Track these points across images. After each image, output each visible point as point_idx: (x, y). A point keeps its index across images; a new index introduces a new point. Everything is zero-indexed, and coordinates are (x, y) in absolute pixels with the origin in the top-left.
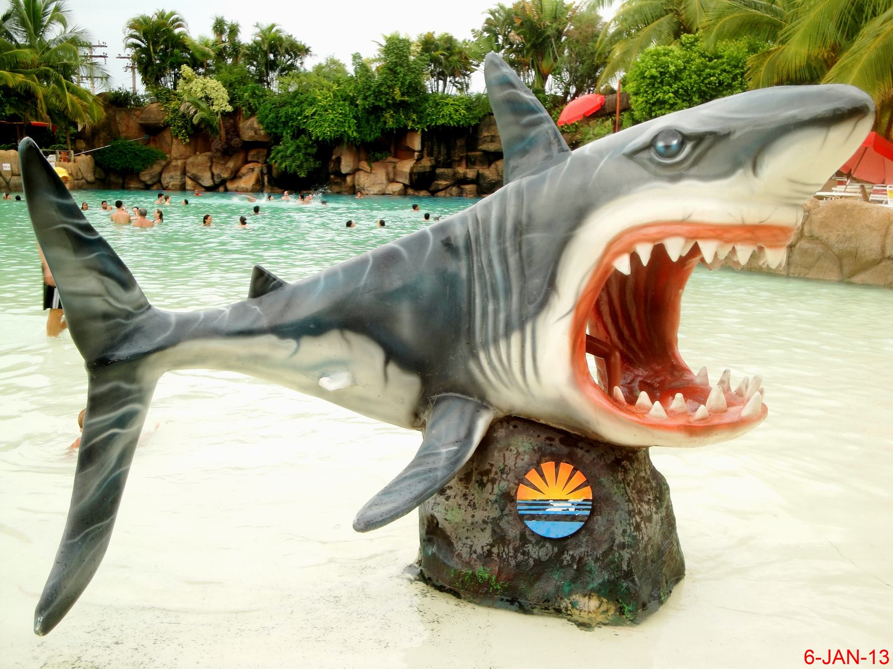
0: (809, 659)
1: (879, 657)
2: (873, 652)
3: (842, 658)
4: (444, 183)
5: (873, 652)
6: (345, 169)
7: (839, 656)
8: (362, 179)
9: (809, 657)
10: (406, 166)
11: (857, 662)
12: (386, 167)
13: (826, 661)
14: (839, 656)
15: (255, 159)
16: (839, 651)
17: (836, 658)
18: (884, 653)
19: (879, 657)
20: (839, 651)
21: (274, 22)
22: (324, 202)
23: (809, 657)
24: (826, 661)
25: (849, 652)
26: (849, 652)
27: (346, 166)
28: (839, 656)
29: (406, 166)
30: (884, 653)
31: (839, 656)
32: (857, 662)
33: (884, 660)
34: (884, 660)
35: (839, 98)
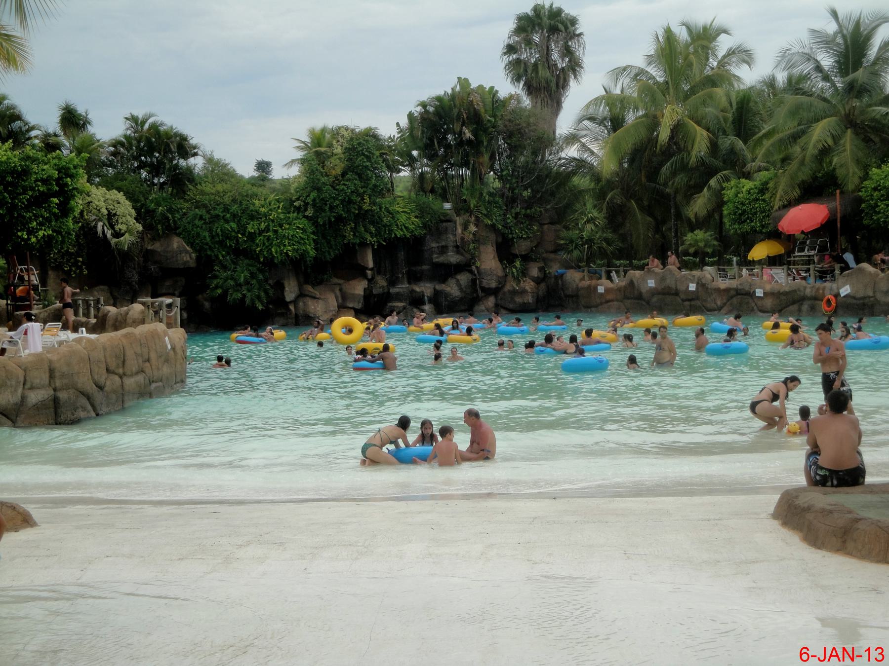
0: (805, 657)
1: (874, 654)
2: (869, 649)
3: (837, 656)
4: (400, 304)
5: (869, 649)
6: (290, 296)
7: (834, 654)
8: (316, 308)
9: (804, 653)
10: (358, 288)
11: (853, 660)
12: (333, 291)
13: (822, 659)
14: (834, 654)
15: (171, 291)
16: (834, 648)
17: (831, 656)
18: (880, 651)
19: (874, 654)
20: (834, 648)
21: (153, 111)
22: (680, 269)
23: (804, 653)
24: (822, 659)
25: (844, 649)
26: (844, 649)
27: (290, 292)
28: (834, 654)
29: (358, 288)
30: (880, 651)
31: (834, 654)
32: (853, 660)
33: (880, 657)
34: (880, 657)
35: (141, 426)
